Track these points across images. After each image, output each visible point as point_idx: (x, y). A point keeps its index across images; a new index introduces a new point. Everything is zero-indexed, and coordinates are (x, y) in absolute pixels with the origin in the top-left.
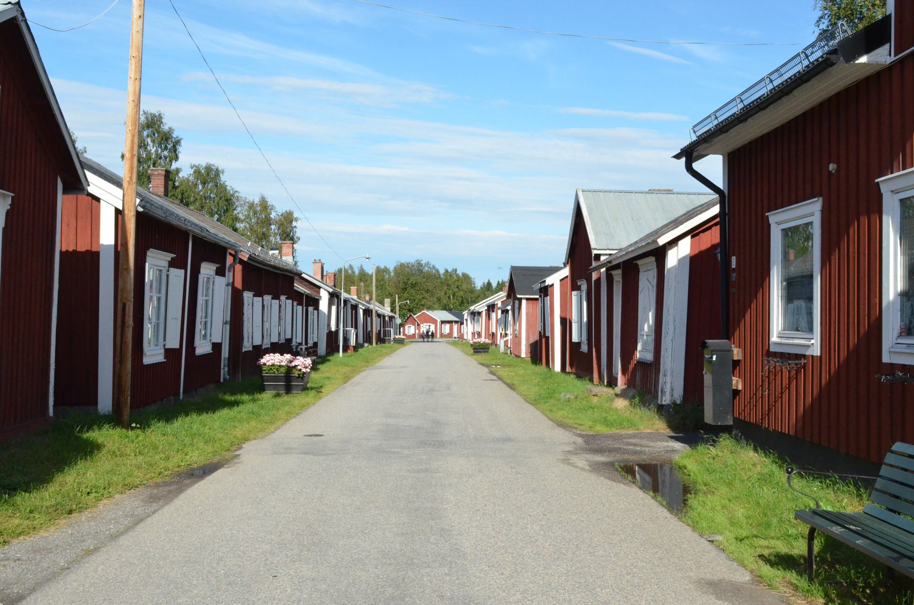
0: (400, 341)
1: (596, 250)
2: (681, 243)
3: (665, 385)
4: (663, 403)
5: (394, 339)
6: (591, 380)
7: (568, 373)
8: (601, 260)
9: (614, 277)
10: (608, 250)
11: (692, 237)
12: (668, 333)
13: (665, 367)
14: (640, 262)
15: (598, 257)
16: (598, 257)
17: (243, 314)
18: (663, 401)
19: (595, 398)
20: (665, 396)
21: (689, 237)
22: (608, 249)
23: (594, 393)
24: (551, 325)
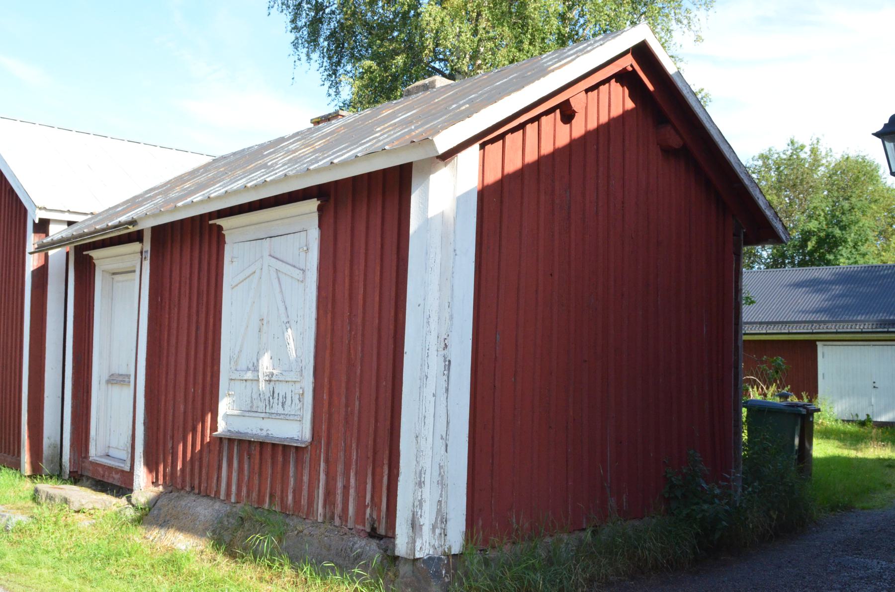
0: (68, 240)
1: (43, 211)
2: (462, 156)
3: (421, 508)
4: (418, 555)
5: (781, 186)
6: (16, 465)
7: (222, 500)
8: (51, 233)
9: (95, 262)
10: (67, 214)
11: (483, 146)
12: (427, 377)
13: (421, 463)
14: (222, 222)
15: (42, 226)
16: (42, 226)
17: (144, 423)
18: (418, 548)
19: (81, 515)
20: (421, 536)
21: (476, 146)
22: (69, 211)
23: (76, 506)
24: (735, 332)
